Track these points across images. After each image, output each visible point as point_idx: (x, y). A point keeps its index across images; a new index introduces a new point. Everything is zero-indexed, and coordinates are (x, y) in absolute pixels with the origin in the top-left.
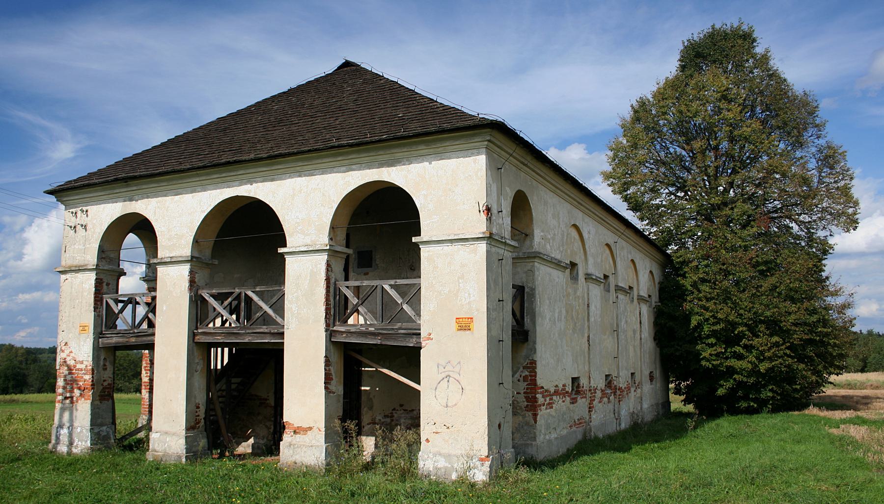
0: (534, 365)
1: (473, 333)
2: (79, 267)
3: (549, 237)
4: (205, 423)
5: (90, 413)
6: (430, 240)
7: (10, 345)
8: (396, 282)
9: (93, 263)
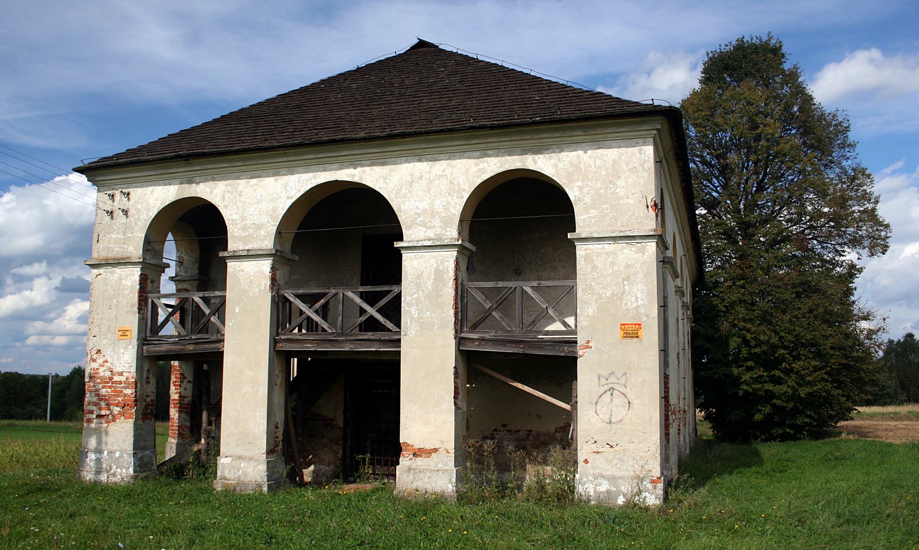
1: (641, 341)
5: (132, 434)
6: (590, 236)
8: (540, 284)
9: (137, 255)
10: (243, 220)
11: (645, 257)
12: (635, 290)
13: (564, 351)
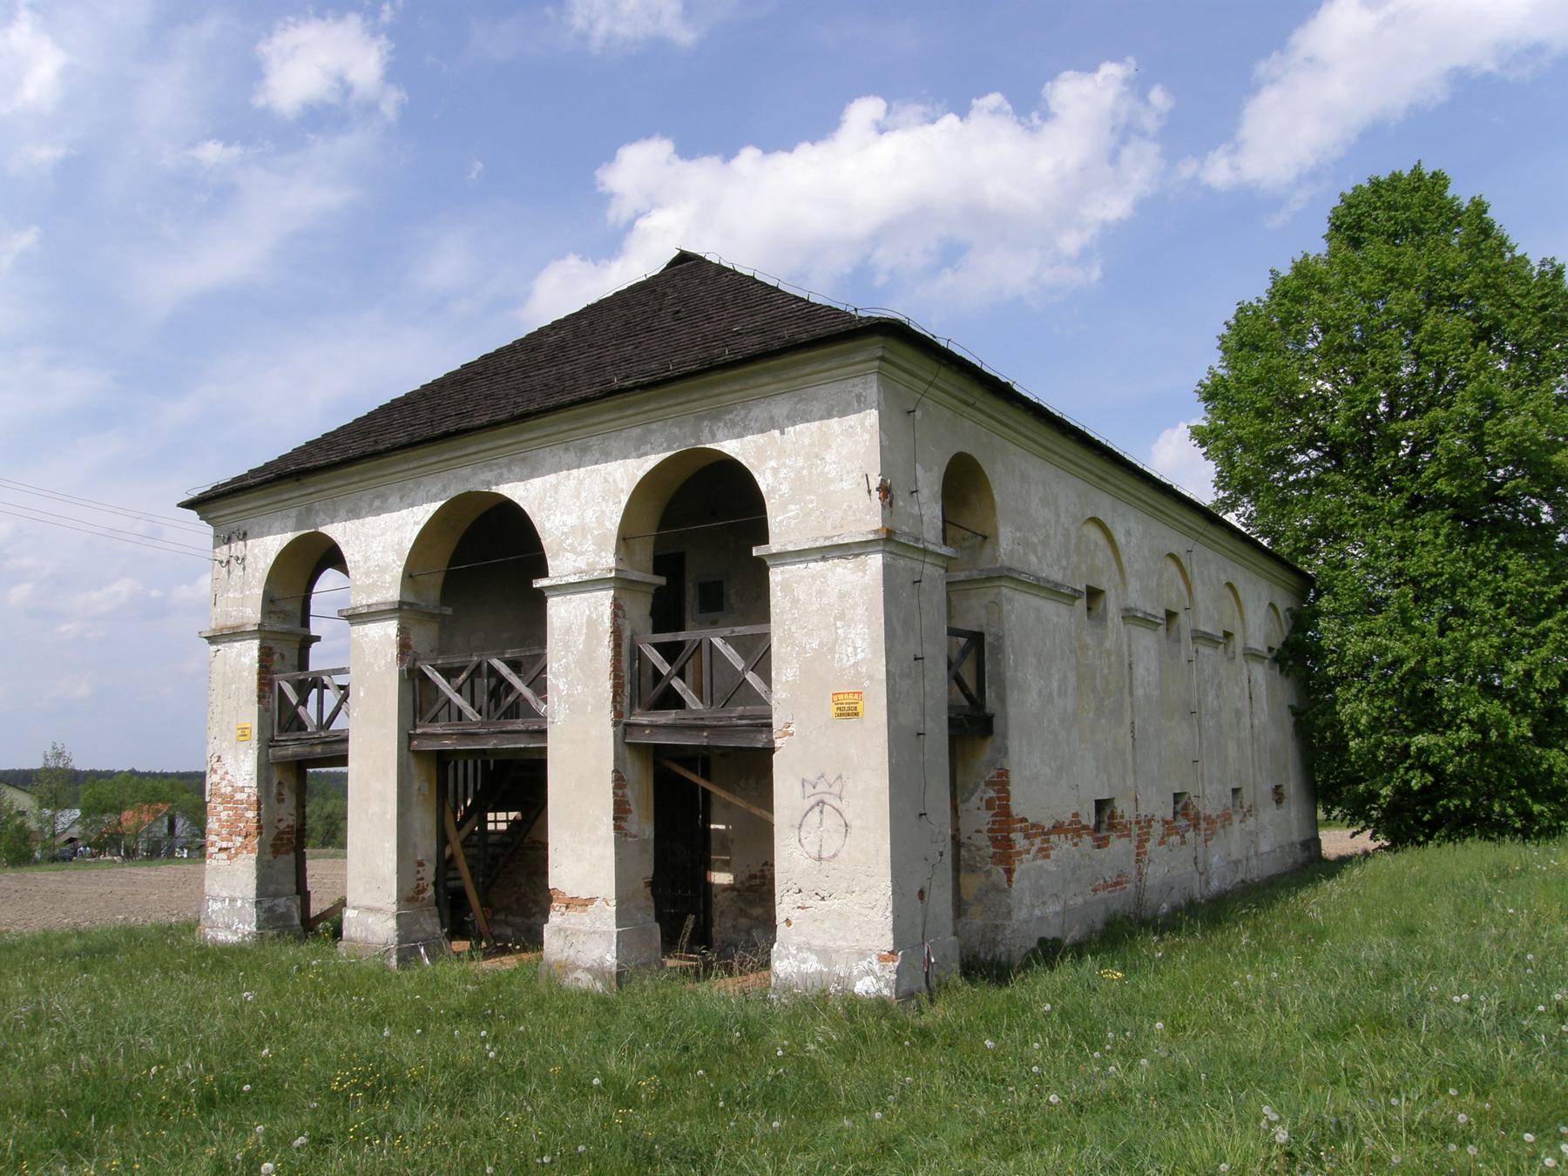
0: (1004, 778)
2: (233, 628)
3: (1035, 540)
4: (436, 892)
8: (733, 632)
10: (365, 562)
11: (867, 577)
12: (853, 636)
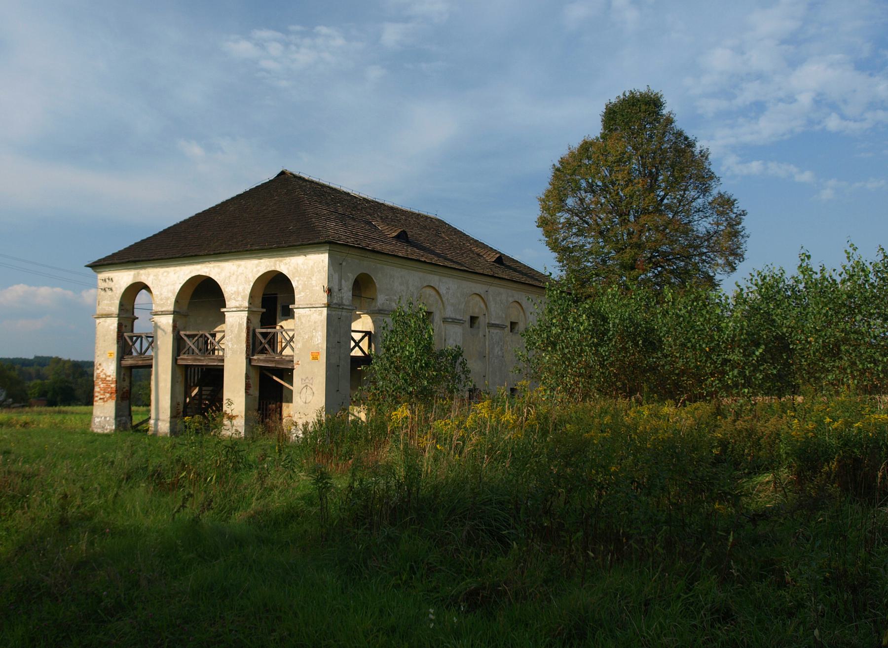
7: (57, 358)
13: (221, 368)
